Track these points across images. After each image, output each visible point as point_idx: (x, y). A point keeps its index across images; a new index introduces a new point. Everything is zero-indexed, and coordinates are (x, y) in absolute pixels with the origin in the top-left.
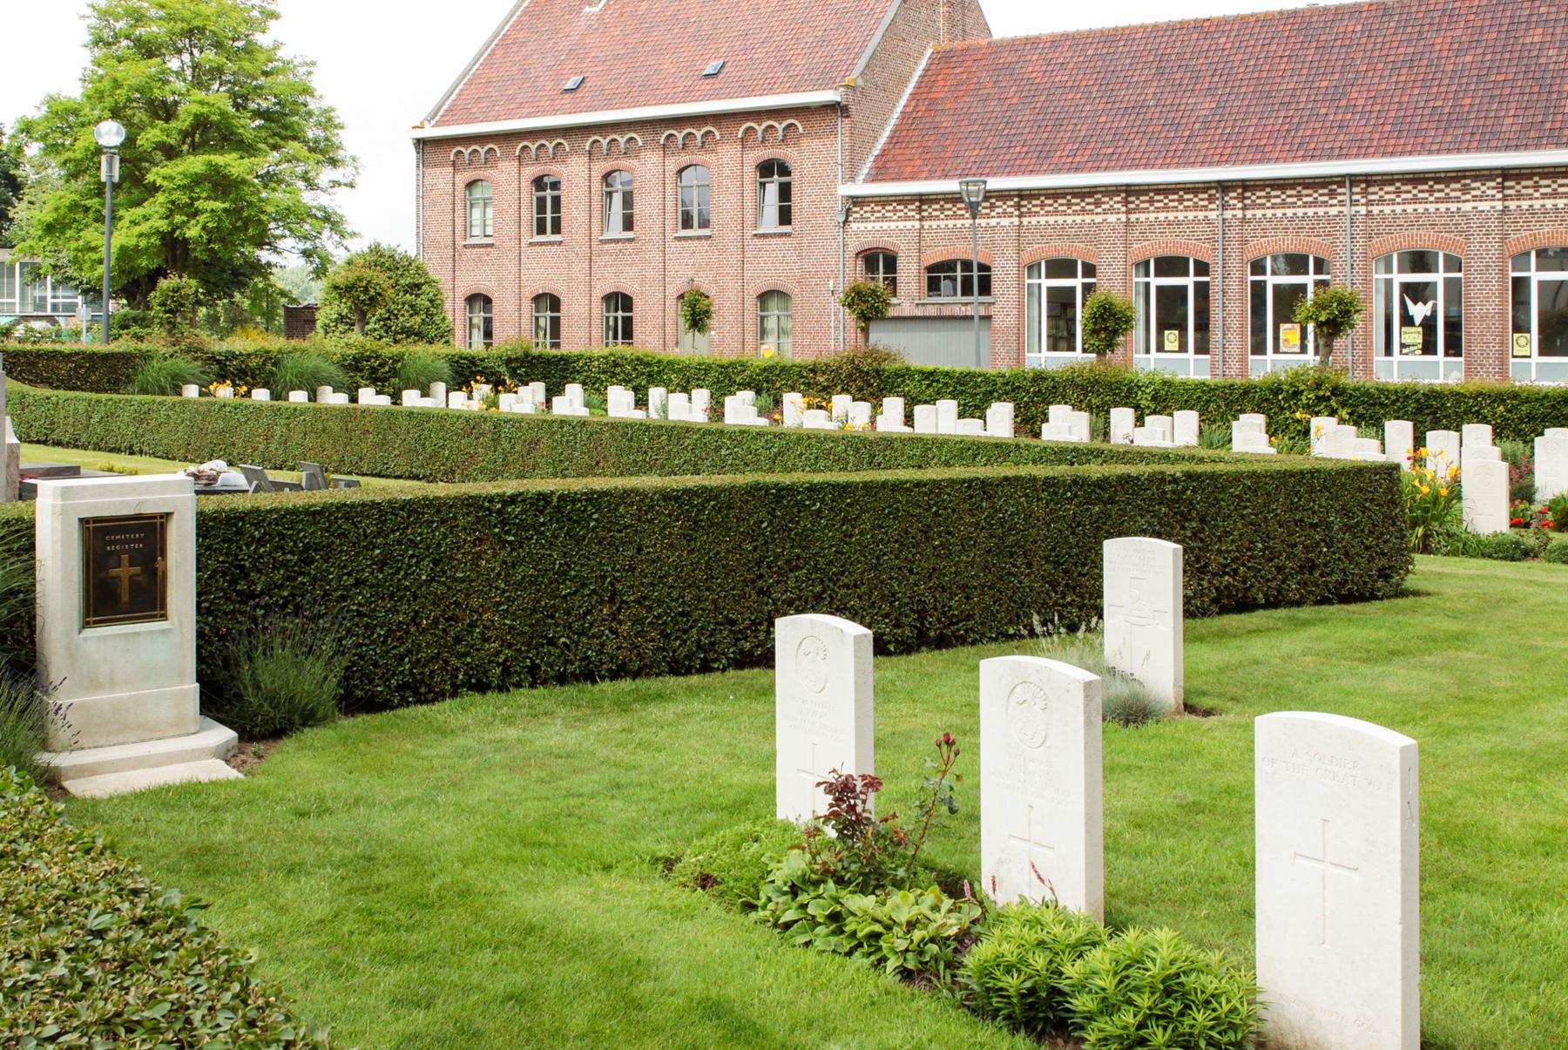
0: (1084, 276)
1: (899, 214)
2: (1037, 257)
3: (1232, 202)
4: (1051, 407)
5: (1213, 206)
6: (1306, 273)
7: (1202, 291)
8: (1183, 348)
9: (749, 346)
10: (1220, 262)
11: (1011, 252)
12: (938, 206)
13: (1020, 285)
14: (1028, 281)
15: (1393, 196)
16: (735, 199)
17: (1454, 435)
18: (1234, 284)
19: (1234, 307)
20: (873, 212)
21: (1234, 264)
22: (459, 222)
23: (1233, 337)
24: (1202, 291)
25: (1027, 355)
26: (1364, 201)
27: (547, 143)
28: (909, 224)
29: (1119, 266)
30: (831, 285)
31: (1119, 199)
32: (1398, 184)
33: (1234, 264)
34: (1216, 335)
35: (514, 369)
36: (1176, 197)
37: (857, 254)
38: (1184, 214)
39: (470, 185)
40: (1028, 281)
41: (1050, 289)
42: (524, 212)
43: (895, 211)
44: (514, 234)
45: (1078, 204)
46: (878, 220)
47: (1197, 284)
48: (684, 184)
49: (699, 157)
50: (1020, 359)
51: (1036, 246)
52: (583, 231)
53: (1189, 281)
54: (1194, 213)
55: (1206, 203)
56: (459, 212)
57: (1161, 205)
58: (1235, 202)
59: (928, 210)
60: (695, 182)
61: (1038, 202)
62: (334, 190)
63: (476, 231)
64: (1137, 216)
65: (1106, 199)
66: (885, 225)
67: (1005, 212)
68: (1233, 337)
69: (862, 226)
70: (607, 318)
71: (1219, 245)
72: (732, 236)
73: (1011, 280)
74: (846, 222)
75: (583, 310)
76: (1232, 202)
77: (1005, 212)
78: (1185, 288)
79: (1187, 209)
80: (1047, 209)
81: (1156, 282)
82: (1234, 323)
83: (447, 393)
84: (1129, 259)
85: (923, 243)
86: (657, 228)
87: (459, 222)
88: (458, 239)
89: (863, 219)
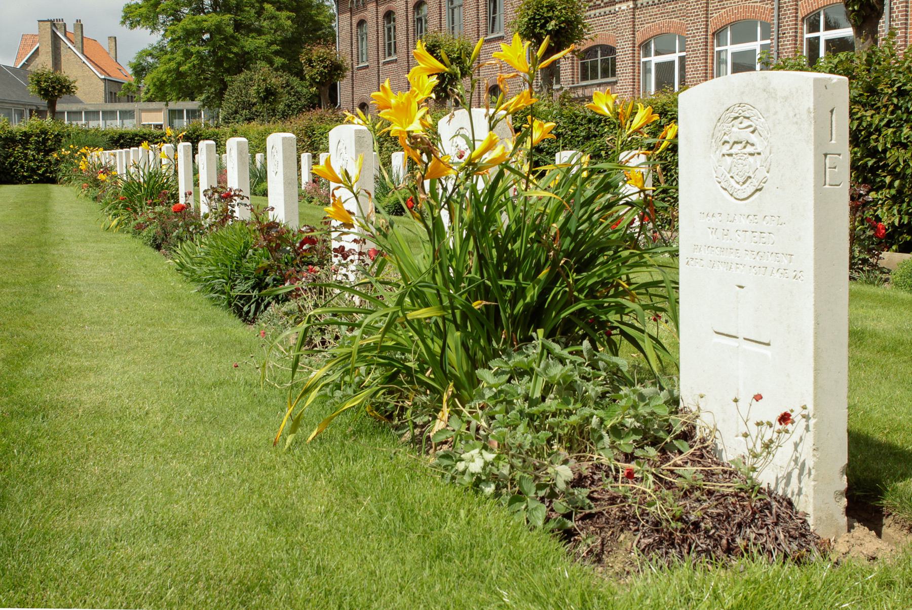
11: (628, 34)
16: (473, 12)
22: (355, 51)
40: (643, 60)
42: (381, 41)
51: (646, 26)
52: (405, 50)
53: (675, 57)
78: (673, 63)
84: (799, 14)
87: (355, 51)
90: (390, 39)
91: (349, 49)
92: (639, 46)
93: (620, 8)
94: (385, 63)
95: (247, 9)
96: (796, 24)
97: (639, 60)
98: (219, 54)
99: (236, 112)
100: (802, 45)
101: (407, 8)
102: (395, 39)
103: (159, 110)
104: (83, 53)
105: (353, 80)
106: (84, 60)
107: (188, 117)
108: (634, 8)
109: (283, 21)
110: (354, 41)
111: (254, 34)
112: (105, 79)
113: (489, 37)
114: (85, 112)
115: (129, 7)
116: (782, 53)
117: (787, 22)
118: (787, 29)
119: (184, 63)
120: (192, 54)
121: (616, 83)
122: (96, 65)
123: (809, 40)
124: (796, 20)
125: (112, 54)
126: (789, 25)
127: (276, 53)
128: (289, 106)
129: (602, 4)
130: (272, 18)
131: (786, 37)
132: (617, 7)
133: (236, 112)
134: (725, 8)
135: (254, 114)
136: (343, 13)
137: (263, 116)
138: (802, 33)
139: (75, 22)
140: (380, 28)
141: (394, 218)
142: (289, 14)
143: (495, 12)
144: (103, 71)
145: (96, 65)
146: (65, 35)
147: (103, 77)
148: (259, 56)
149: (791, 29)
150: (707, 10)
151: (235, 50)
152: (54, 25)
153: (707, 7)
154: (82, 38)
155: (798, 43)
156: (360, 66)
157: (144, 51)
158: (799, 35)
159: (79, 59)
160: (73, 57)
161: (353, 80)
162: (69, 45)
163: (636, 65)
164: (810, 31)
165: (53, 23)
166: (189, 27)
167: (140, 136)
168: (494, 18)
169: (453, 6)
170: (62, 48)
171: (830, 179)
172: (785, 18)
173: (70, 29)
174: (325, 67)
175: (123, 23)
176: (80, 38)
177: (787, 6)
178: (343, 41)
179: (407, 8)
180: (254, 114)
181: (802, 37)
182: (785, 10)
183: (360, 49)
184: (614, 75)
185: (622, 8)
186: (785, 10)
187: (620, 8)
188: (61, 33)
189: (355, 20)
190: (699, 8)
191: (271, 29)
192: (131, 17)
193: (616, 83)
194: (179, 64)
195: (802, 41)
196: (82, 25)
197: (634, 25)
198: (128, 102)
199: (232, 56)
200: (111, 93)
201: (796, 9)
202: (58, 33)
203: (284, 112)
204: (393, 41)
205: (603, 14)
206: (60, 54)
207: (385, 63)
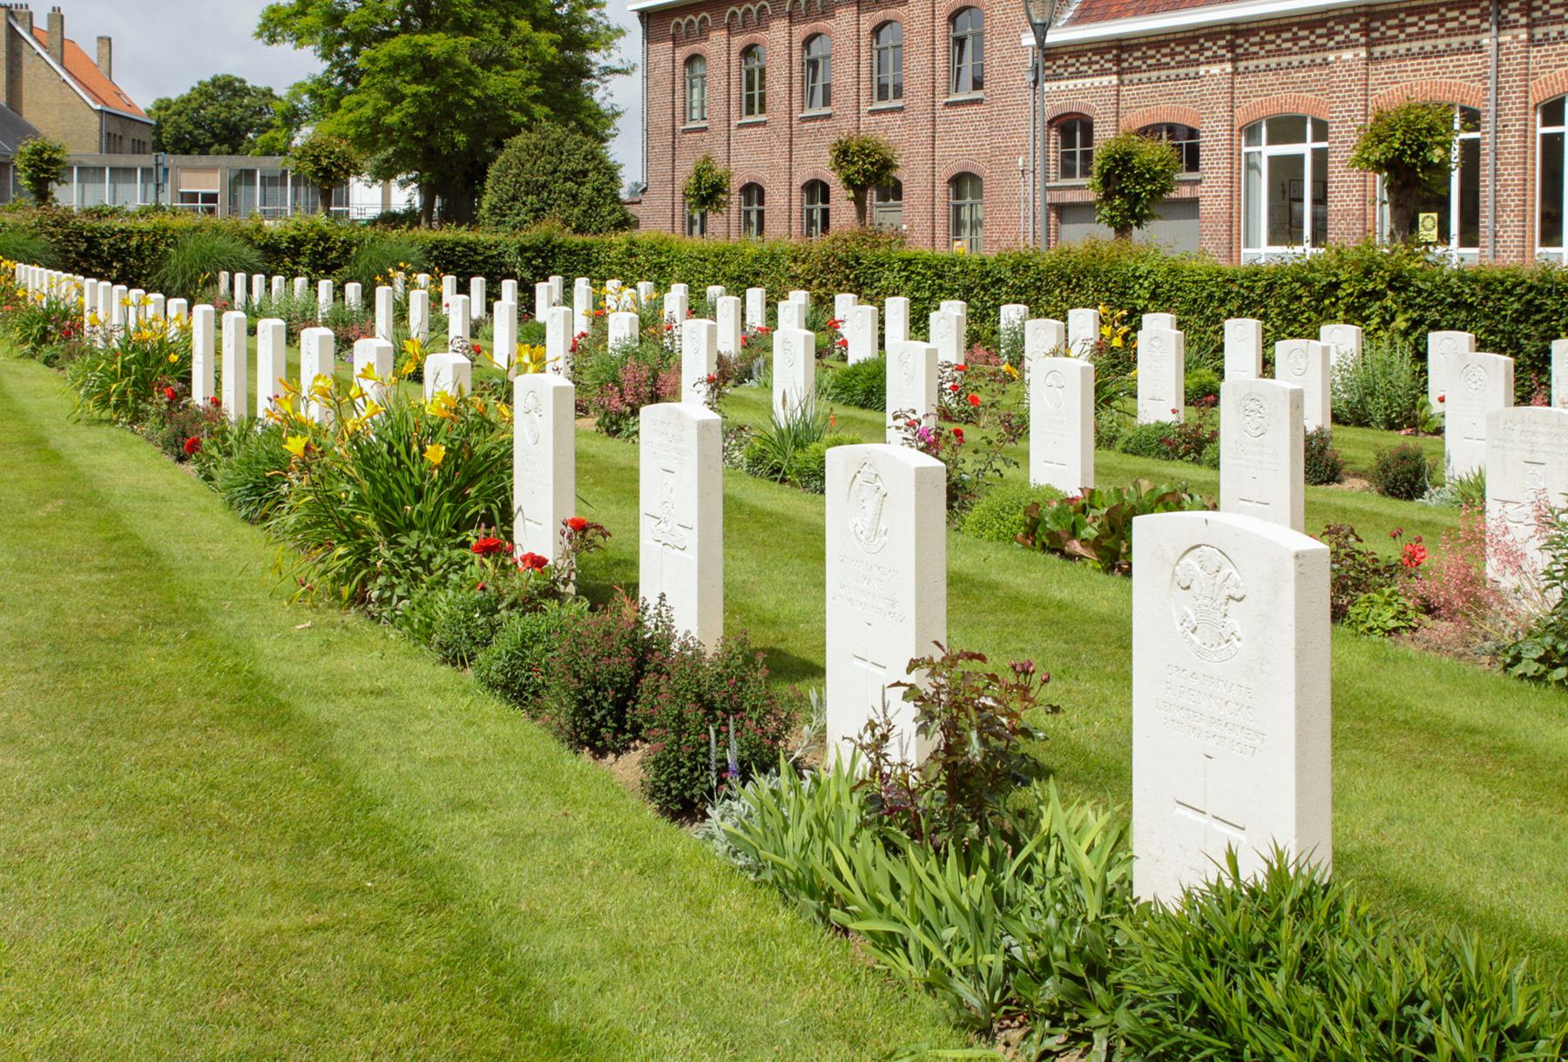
0: (1315, 139)
1: (1179, 58)
2: (1256, 115)
3: (1512, 17)
4: (1554, 342)
5: (1485, 25)
6: (1303, 140)
7: (1320, 158)
8: (1444, 235)
9: (940, 243)
10: (1492, 108)
11: (1222, 111)
12: (1139, 54)
13: (1232, 155)
14: (1245, 149)
15: (1435, 27)
16: (925, 60)
17: (1054, 324)
18: (1512, 140)
19: (1511, 175)
20: (1066, 66)
21: (1513, 109)
22: (679, 103)
23: (1510, 219)
24: (1320, 158)
25: (1244, 250)
26: (1115, 69)
27: (680, 20)
28: (1105, 80)
29: (1222, 131)
30: (1021, 163)
31: (1356, 26)
32: (1443, 10)
33: (1513, 109)
34: (1486, 221)
35: (529, 260)
36: (1435, 17)
37: (1050, 123)
38: (1446, 40)
39: (877, 31)
40: (1245, 149)
41: (1271, 158)
42: (733, 90)
43: (1090, 63)
44: (723, 116)
45: (1306, 38)
46: (1072, 76)
47: (1315, 152)
48: (882, 45)
49: (822, 25)
50: (1232, 251)
51: (1254, 100)
52: (784, 108)
53: (1305, 149)
54: (1460, 39)
55: (1477, 22)
56: (679, 94)
57: (1415, 29)
58: (1516, 16)
59: (1130, 60)
60: (891, 42)
61: (1257, 39)
62: (607, 78)
63: (696, 114)
64: (1381, 49)
65: (1341, 28)
66: (1079, 82)
67: (1215, 56)
68: (1510, 219)
69: (1054, 85)
70: (810, 212)
71: (1491, 84)
72: (922, 105)
73: (1222, 149)
74: (1036, 82)
75: (783, 201)
76: (1512, 17)
77: (1215, 56)
78: (1300, 158)
79: (1450, 33)
80: (1268, 47)
81: (1267, 151)
82: (1512, 199)
83: (1267, 345)
84: (1530, 100)
85: (1122, 104)
86: (852, 102)
87: (679, 103)
88: (677, 123)
89: (1057, 77)
90: (750, 87)
91: (670, 98)
92: (1240, 130)
93: (1207, 72)
94: (740, 126)
95: (489, 26)
96: (1526, 114)
97: (1240, 150)
98: (450, 99)
99: (514, 198)
100: (1534, 143)
101: (791, 43)
102: (762, 87)
103: (213, 169)
104: (62, 65)
105: (674, 148)
106: (64, 76)
107: (263, 184)
108: (1233, 74)
109: (543, 47)
110: (678, 86)
111: (498, 68)
112: (101, 111)
113: (951, 99)
114: (79, 168)
115: (274, 11)
116: (1503, 154)
117: (1511, 109)
118: (1510, 120)
119: (389, 110)
120: (403, 97)
121: (1199, 182)
122: (84, 85)
123: (1545, 137)
124: (1526, 108)
125: (104, 67)
126: (1514, 114)
127: (535, 99)
128: (599, 191)
129: (1173, 64)
130: (525, 42)
131: (1510, 131)
132: (1202, 70)
133: (514, 198)
134: (1398, 83)
135: (545, 202)
136: (658, 41)
137: (559, 206)
138: (1534, 126)
139: (50, 11)
140: (734, 70)
141: (549, 367)
142: (552, 36)
143: (960, 62)
144: (97, 97)
145: (84, 85)
146: (31, 33)
147: (98, 107)
148: (511, 103)
149: (1517, 120)
150: (1367, 85)
151: (477, 93)
152: (12, 14)
153: (1367, 79)
154: (63, 39)
155: (1529, 140)
156: (687, 126)
157: (300, 85)
158: (1530, 129)
159: (55, 76)
160: (43, 70)
161: (674, 148)
162: (39, 49)
163: (1235, 157)
164: (1545, 123)
165: (10, 12)
166: (398, 53)
167: (465, 246)
168: (959, 69)
169: (879, 46)
170: (25, 55)
171: (254, 196)
172: (1507, 104)
173: (41, 23)
174: (872, 164)
175: (259, 35)
176: (58, 38)
177: (1511, 87)
178: (656, 84)
179: (791, 43)
180: (545, 202)
181: (1534, 132)
182: (1507, 93)
183: (688, 100)
184: (762, 110)
185: (1212, 72)
186: (1507, 93)
187: (1207, 72)
188: (24, 28)
189: (682, 53)
190: (1353, 81)
191: (525, 59)
192: (274, 27)
193: (1199, 182)
194: (380, 112)
195: (1534, 137)
196: (62, 17)
197: (1233, 98)
198: (133, 152)
199: (471, 102)
200: (109, 134)
201: (1527, 92)
202: (19, 29)
203: (592, 199)
204: (757, 92)
205: (1163, 78)
206: (20, 65)
207: (740, 126)
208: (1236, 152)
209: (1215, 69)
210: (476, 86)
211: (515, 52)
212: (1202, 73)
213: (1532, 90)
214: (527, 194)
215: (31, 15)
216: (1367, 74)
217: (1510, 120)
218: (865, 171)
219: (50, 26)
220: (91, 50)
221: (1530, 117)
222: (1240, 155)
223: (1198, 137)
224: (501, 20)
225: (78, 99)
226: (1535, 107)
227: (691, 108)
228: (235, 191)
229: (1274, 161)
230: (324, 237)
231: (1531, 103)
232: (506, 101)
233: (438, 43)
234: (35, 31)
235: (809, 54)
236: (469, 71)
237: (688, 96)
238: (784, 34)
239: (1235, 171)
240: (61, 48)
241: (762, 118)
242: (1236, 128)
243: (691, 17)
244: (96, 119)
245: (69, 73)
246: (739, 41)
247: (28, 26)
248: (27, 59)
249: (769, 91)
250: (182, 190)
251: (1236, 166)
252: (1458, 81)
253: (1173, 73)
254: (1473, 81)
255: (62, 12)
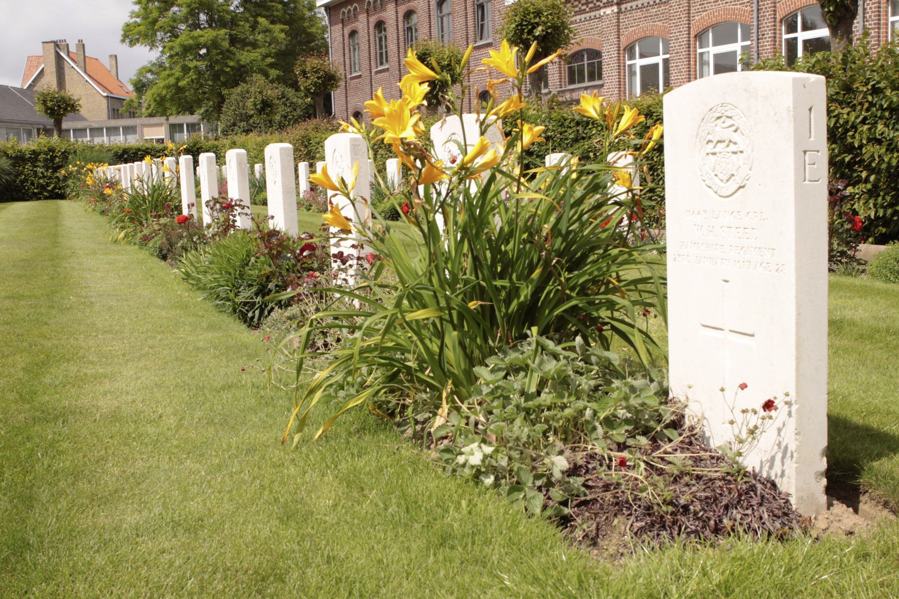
11: (613, 38)
13: (620, 66)
16: (462, 20)
22: (347, 62)
33: (767, 23)
40: (628, 63)
44: (368, 67)
51: (631, 29)
52: (396, 59)
87: (347, 62)
88: (348, 74)
90: (381, 48)
92: (624, 50)
93: (605, 13)
94: (377, 72)
95: (242, 23)
97: (625, 63)
98: (216, 68)
99: (234, 124)
100: (781, 45)
101: (397, 18)
102: (386, 48)
104: (85, 72)
106: (87, 78)
108: (618, 13)
109: (276, 34)
110: (347, 51)
112: (107, 97)
116: (762, 54)
117: (766, 23)
118: (766, 31)
120: (190, 69)
121: (602, 86)
122: (98, 83)
123: (787, 40)
124: (775, 21)
126: (768, 27)
127: (271, 65)
128: (285, 117)
129: (587, 10)
130: (266, 31)
131: (766, 38)
132: (602, 12)
133: (234, 124)
137: (260, 127)
138: (781, 34)
139: (77, 42)
143: (483, 19)
144: (105, 88)
145: (98, 83)
146: (68, 55)
147: (105, 94)
148: (255, 68)
149: (770, 30)
151: (232, 64)
152: (58, 45)
154: (85, 57)
155: (777, 43)
158: (778, 36)
159: (82, 79)
160: (76, 76)
162: (73, 64)
163: (622, 68)
164: (788, 32)
167: (143, 151)
168: (482, 25)
170: (66, 68)
172: (764, 20)
173: (73, 49)
174: (318, 78)
176: (82, 57)
177: (766, 8)
181: (781, 38)
182: (764, 12)
183: (352, 59)
185: (607, 13)
186: (764, 12)
187: (605, 13)
188: (64, 53)
189: (347, 31)
191: (266, 42)
195: (781, 41)
199: (228, 70)
200: (114, 109)
202: (62, 54)
203: (280, 123)
204: (384, 50)
205: (583, 19)
207: (377, 72)
208: (622, 65)
209: (608, 11)
210: (232, 60)
211: (260, 37)
212: (602, 14)
213: (778, 10)
214: (241, 121)
215: (68, 45)
216: (689, 6)
217: (766, 31)
218: (316, 83)
219: (77, 50)
220: (107, 62)
221: (778, 28)
222: (624, 66)
223: (601, 57)
224: (251, 19)
225: (95, 91)
226: (781, 21)
227: (355, 64)
228: (173, 136)
229: (644, 68)
230: (52, 150)
231: (778, 18)
232: (251, 68)
233: (207, 35)
234: (70, 54)
235: (408, 23)
236: (228, 51)
237: (352, 57)
238: (393, 12)
239: (622, 77)
240: (85, 62)
241: (386, 67)
242: (622, 49)
243: (349, 7)
244: (105, 101)
245: (90, 76)
246: (373, 19)
247: (66, 51)
248: (67, 71)
249: (389, 49)
250: (146, 138)
251: (622, 74)
252: (738, 6)
253: (587, 15)
254: (746, 6)
255: (84, 42)
